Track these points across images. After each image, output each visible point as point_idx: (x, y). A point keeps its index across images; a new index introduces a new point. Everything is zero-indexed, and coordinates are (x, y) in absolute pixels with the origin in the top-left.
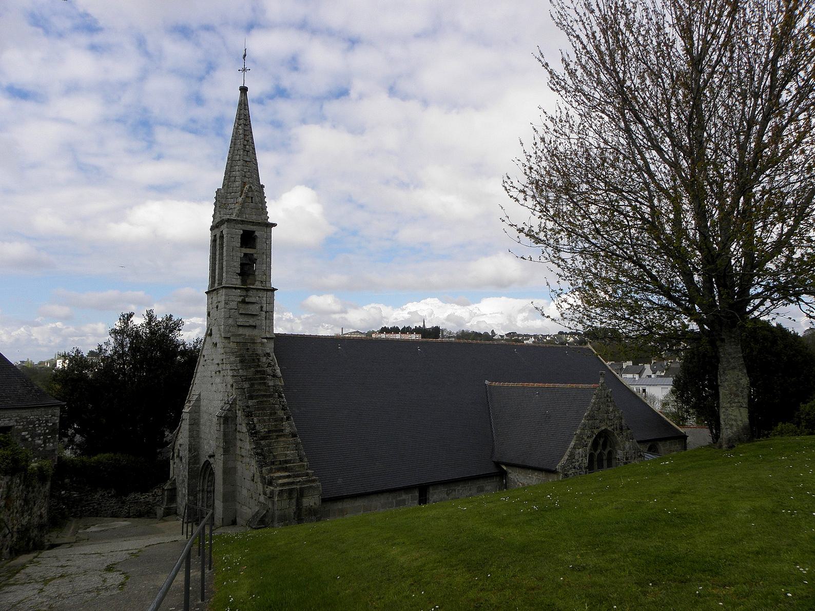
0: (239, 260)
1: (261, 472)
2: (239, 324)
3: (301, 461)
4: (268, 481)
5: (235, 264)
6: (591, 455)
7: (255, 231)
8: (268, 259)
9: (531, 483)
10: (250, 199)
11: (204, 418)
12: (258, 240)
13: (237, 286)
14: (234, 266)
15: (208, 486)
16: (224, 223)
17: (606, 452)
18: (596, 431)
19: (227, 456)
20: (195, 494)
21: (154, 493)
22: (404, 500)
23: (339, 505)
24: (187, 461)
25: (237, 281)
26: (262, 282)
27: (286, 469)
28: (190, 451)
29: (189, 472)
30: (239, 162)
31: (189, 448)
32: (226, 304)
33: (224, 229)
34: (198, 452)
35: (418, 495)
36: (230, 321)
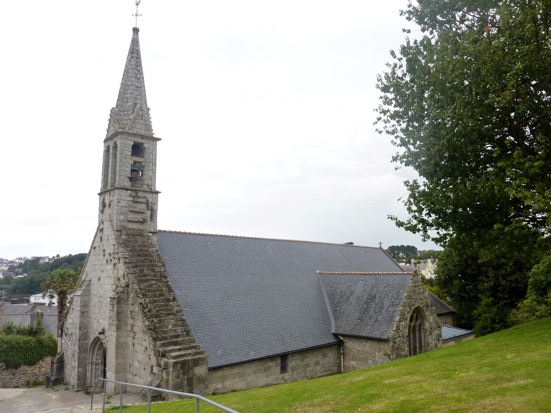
0: (130, 166)
1: (155, 346)
2: (129, 219)
3: (188, 336)
4: (162, 354)
5: (127, 169)
6: (410, 326)
7: (144, 143)
8: (154, 167)
9: (365, 350)
10: (141, 117)
11: (94, 300)
12: (146, 151)
13: (128, 188)
14: (126, 171)
15: (96, 359)
16: (118, 135)
17: (418, 323)
18: (413, 308)
19: (120, 332)
20: (85, 366)
21: (39, 365)
22: (270, 367)
23: (220, 373)
24: (78, 338)
25: (128, 184)
26: (148, 185)
27: (176, 344)
28: (80, 328)
29: (79, 347)
30: (131, 87)
31: (80, 326)
32: (119, 202)
33: (119, 140)
34: (87, 329)
35: (280, 362)
36: (122, 217)
